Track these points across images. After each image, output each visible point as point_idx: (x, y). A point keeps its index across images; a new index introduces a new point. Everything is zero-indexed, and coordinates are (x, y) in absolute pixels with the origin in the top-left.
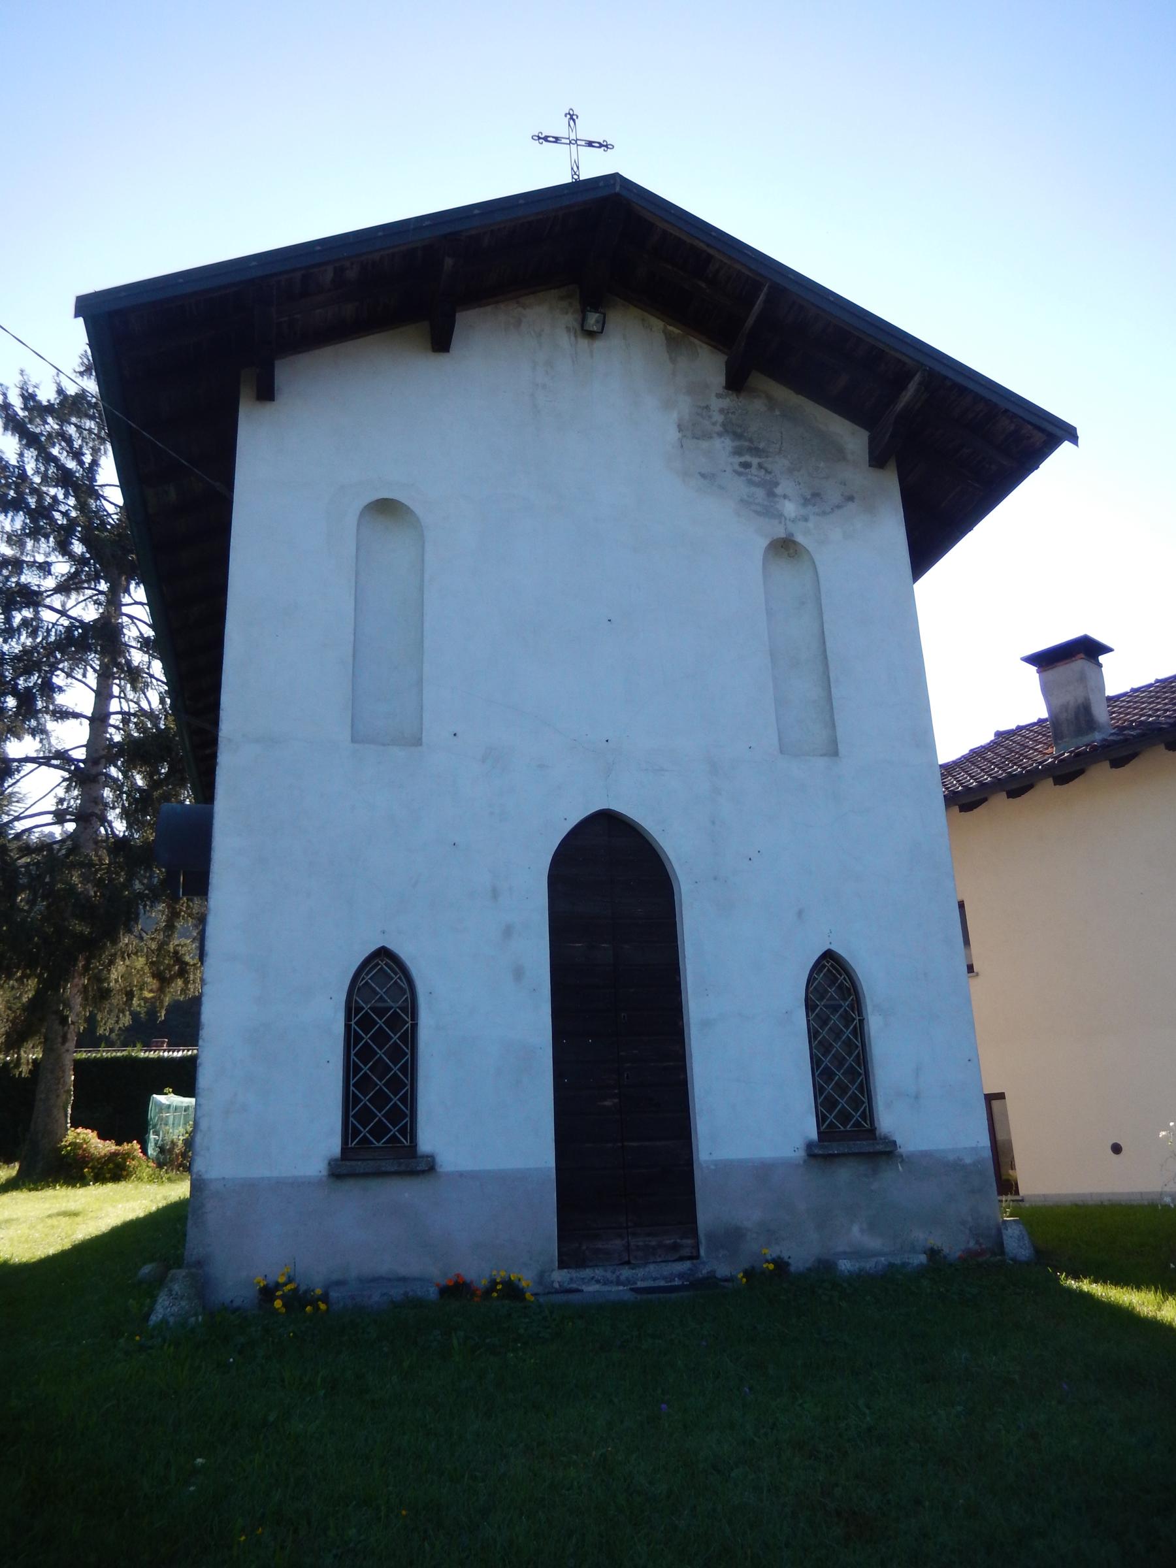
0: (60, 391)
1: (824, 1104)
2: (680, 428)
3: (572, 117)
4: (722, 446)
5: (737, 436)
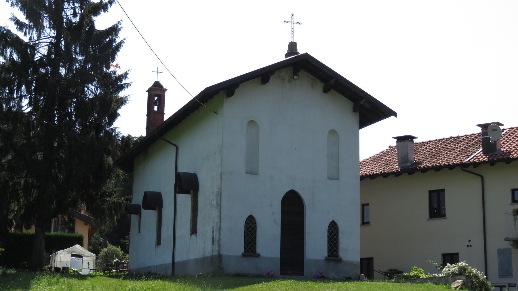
1: (329, 250)
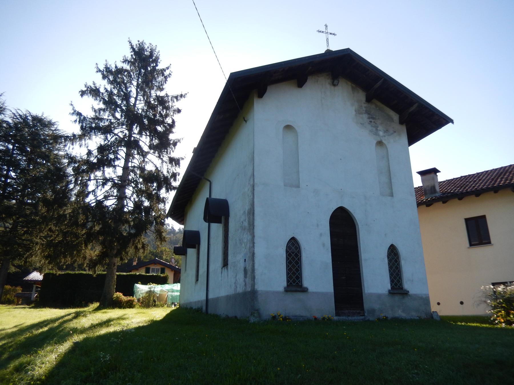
0: (116, 67)
1: (392, 281)
2: (355, 111)
3: (326, 26)
4: (365, 116)
5: (369, 114)
